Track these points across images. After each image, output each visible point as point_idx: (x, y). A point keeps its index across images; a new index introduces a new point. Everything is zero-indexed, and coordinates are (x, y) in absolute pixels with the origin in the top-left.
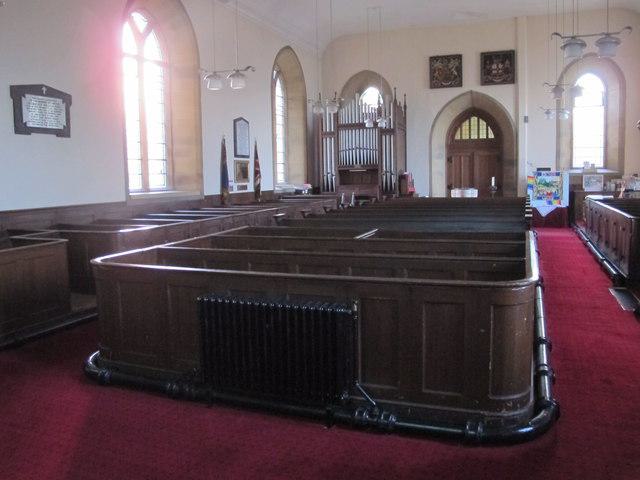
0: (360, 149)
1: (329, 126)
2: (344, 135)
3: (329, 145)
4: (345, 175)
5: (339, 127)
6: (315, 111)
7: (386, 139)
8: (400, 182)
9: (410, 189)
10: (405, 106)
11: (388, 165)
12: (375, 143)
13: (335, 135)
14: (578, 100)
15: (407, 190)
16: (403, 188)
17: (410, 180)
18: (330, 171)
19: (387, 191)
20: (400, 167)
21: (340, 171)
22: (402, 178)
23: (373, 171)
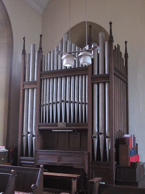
0: (75, 103)
1: (32, 75)
2: (49, 85)
3: (31, 97)
4: (47, 137)
5: (45, 75)
6: (66, 65)
7: (100, 89)
8: (117, 146)
9: (132, 159)
10: (126, 55)
11: (100, 123)
12: (83, 96)
13: (39, 85)
14: (113, 43)
15: (128, 159)
16: (122, 157)
17: (132, 145)
18: (30, 127)
19: (99, 161)
20: (119, 126)
21: (40, 130)
22: (121, 143)
23: (80, 130)
